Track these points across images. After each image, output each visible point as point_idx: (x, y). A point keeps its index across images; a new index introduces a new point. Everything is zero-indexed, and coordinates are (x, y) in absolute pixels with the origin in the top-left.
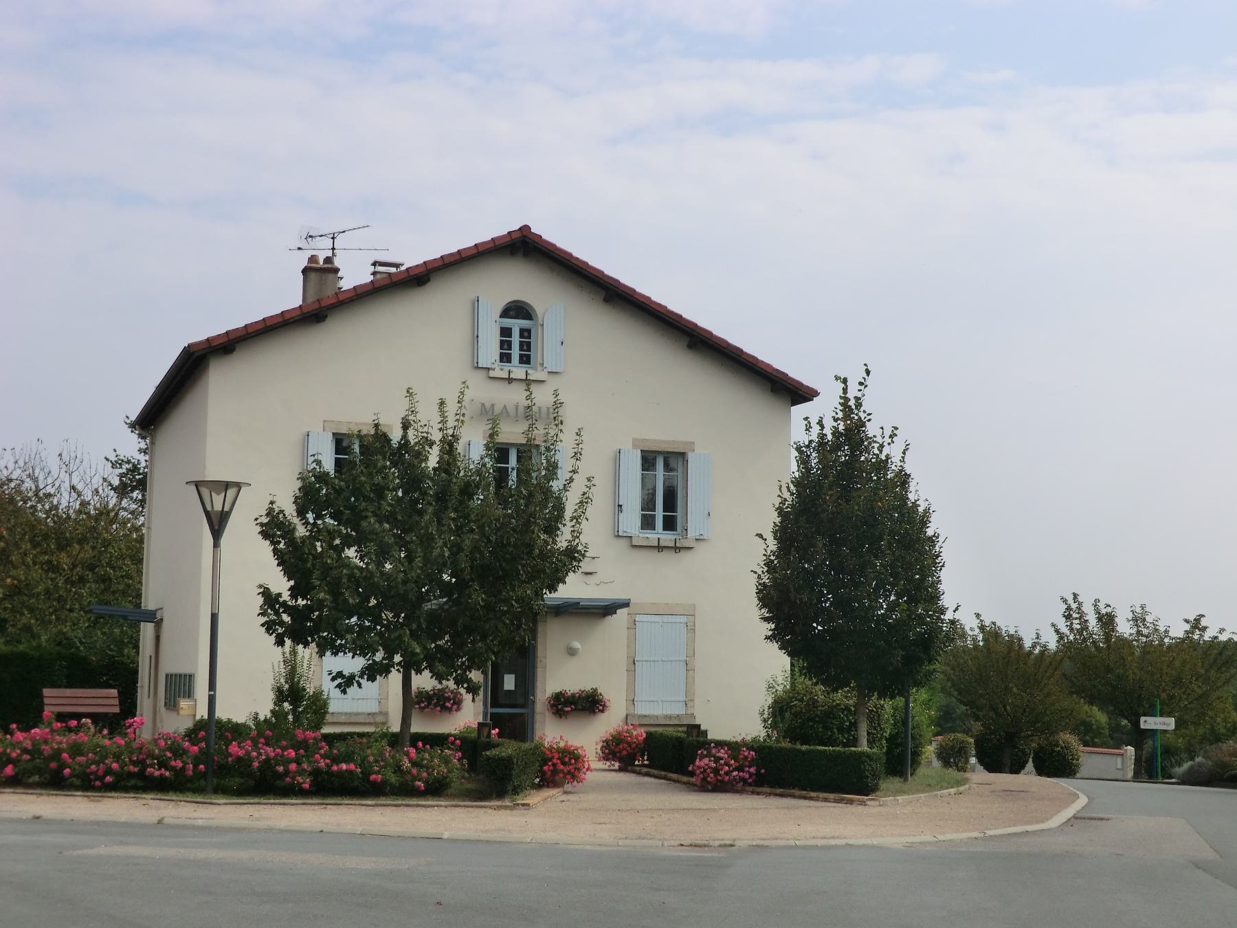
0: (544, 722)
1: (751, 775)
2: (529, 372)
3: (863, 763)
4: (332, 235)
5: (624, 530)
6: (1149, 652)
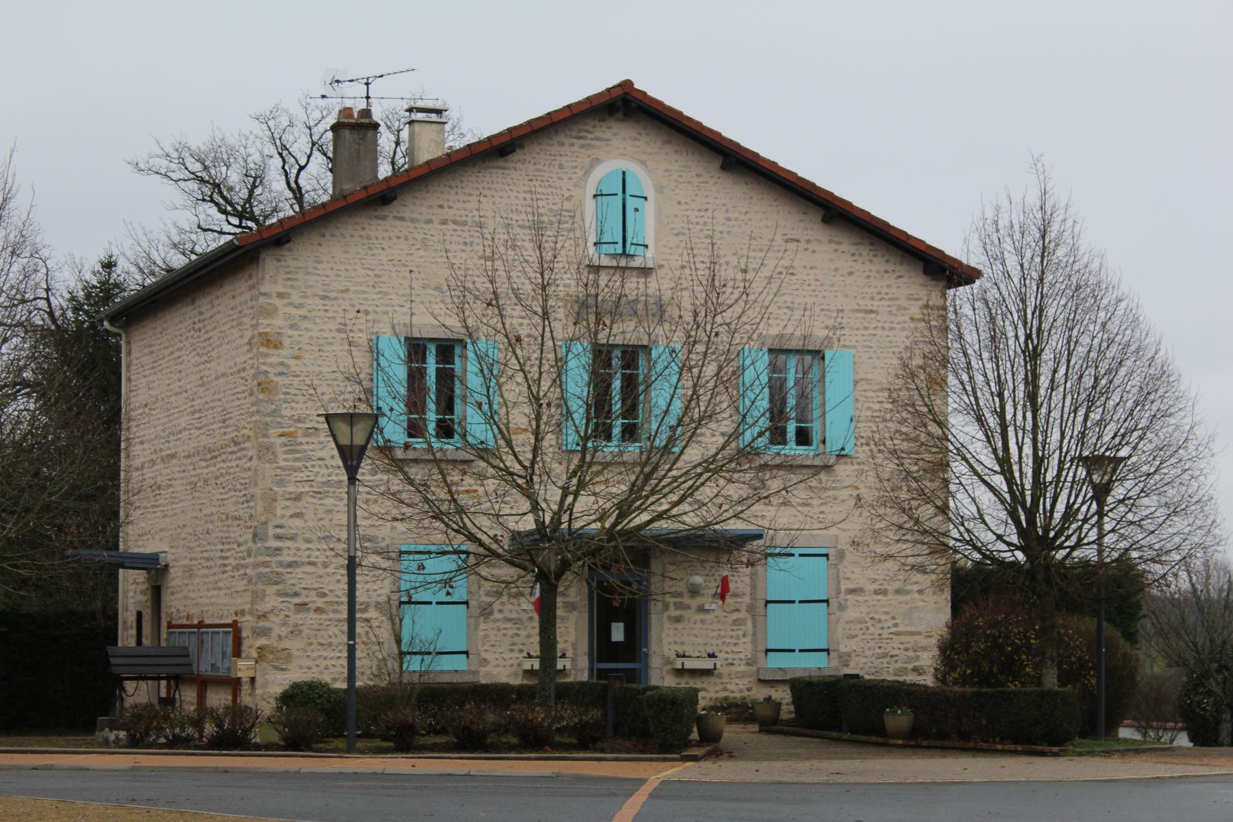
4: (365, 81)
6: (1136, 642)
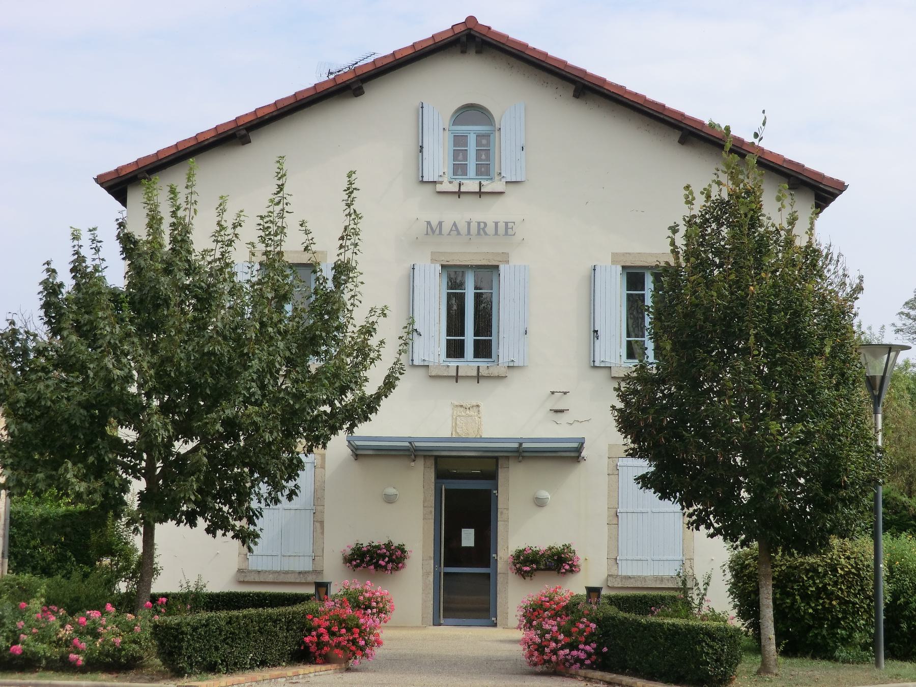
0: (507, 583)
1: (589, 655)
2: (483, 183)
3: (699, 643)
5: (602, 360)
